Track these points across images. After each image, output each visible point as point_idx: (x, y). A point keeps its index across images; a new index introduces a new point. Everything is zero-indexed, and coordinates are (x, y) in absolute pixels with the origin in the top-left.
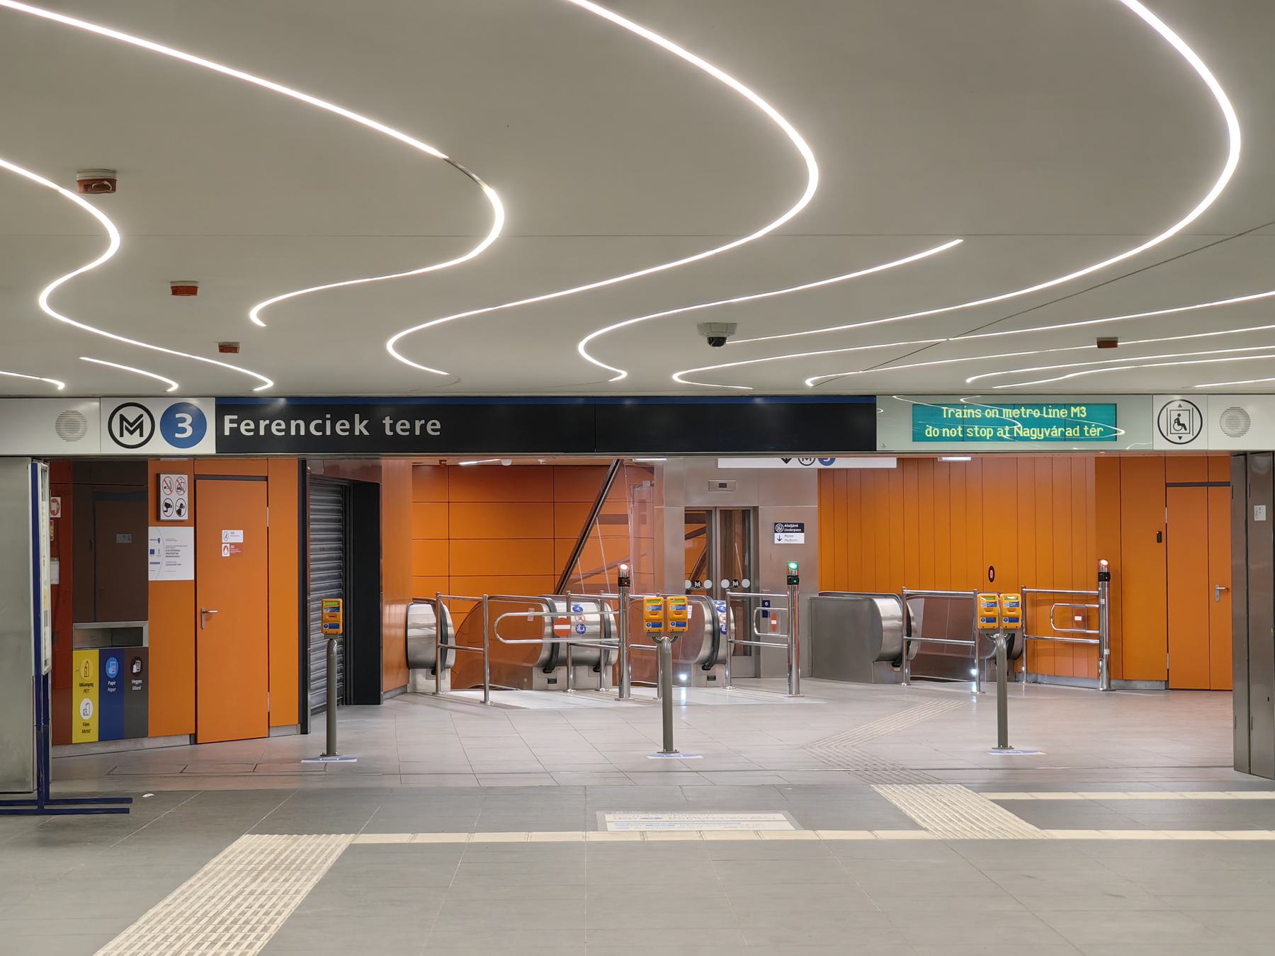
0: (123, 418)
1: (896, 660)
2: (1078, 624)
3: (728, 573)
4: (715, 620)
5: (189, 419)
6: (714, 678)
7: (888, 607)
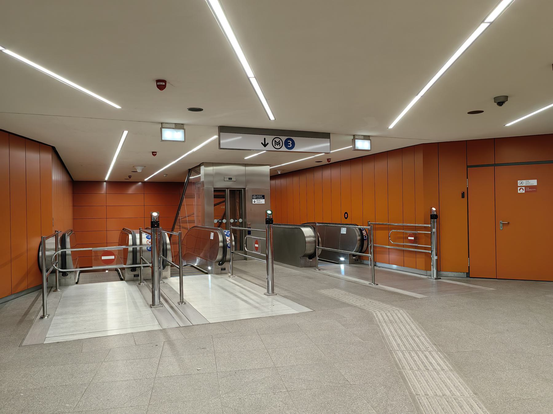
1: (312, 256)
3: (234, 216)
4: (224, 241)
6: (225, 269)
7: (308, 231)
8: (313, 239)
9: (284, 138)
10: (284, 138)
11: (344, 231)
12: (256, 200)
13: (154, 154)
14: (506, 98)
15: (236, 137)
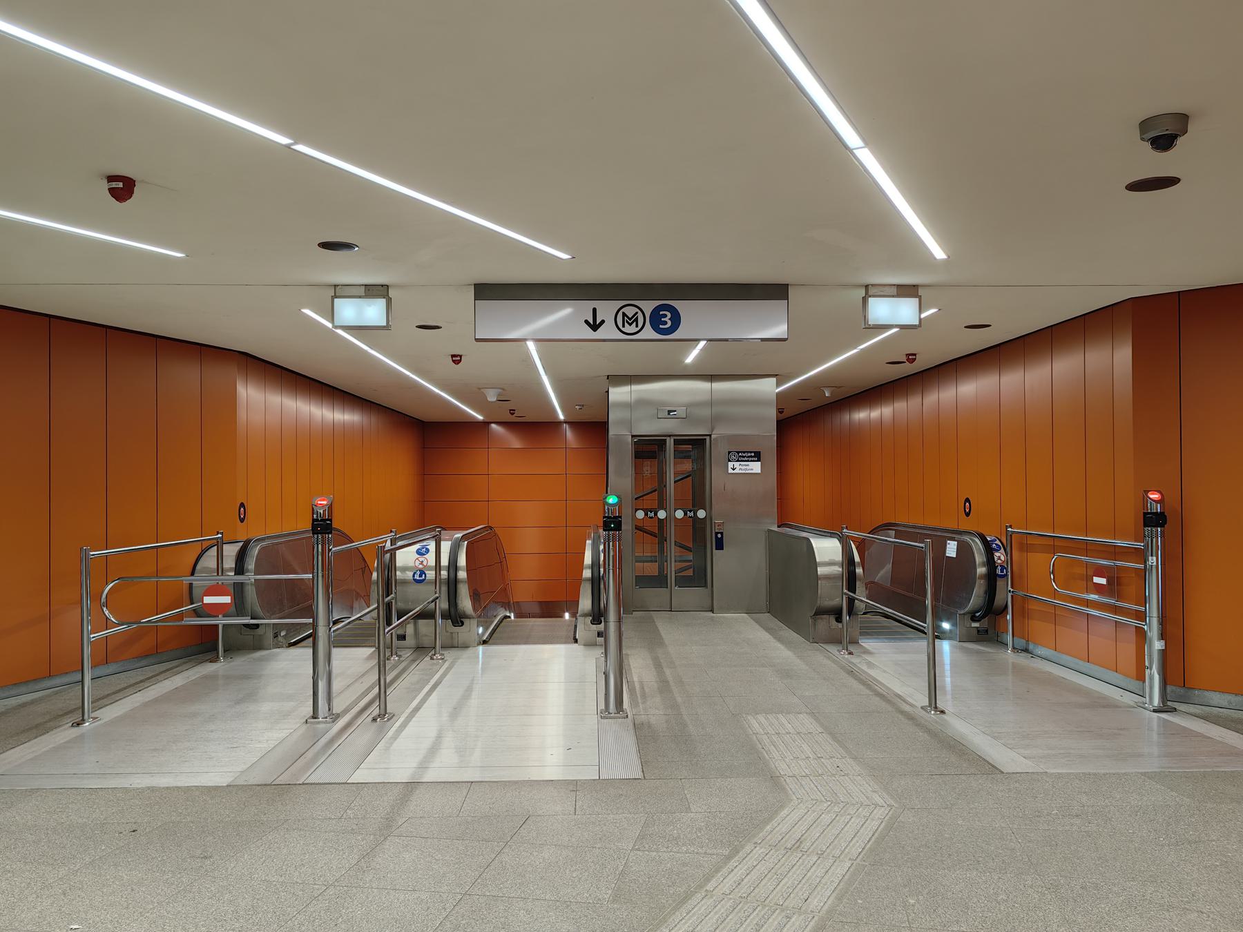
0: (624, 315)
2: (1099, 589)
5: (669, 315)
8: (837, 569)
9: (648, 306)
10: (648, 306)
12: (737, 464)
13: (457, 359)
14: (1182, 120)
15: (564, 308)
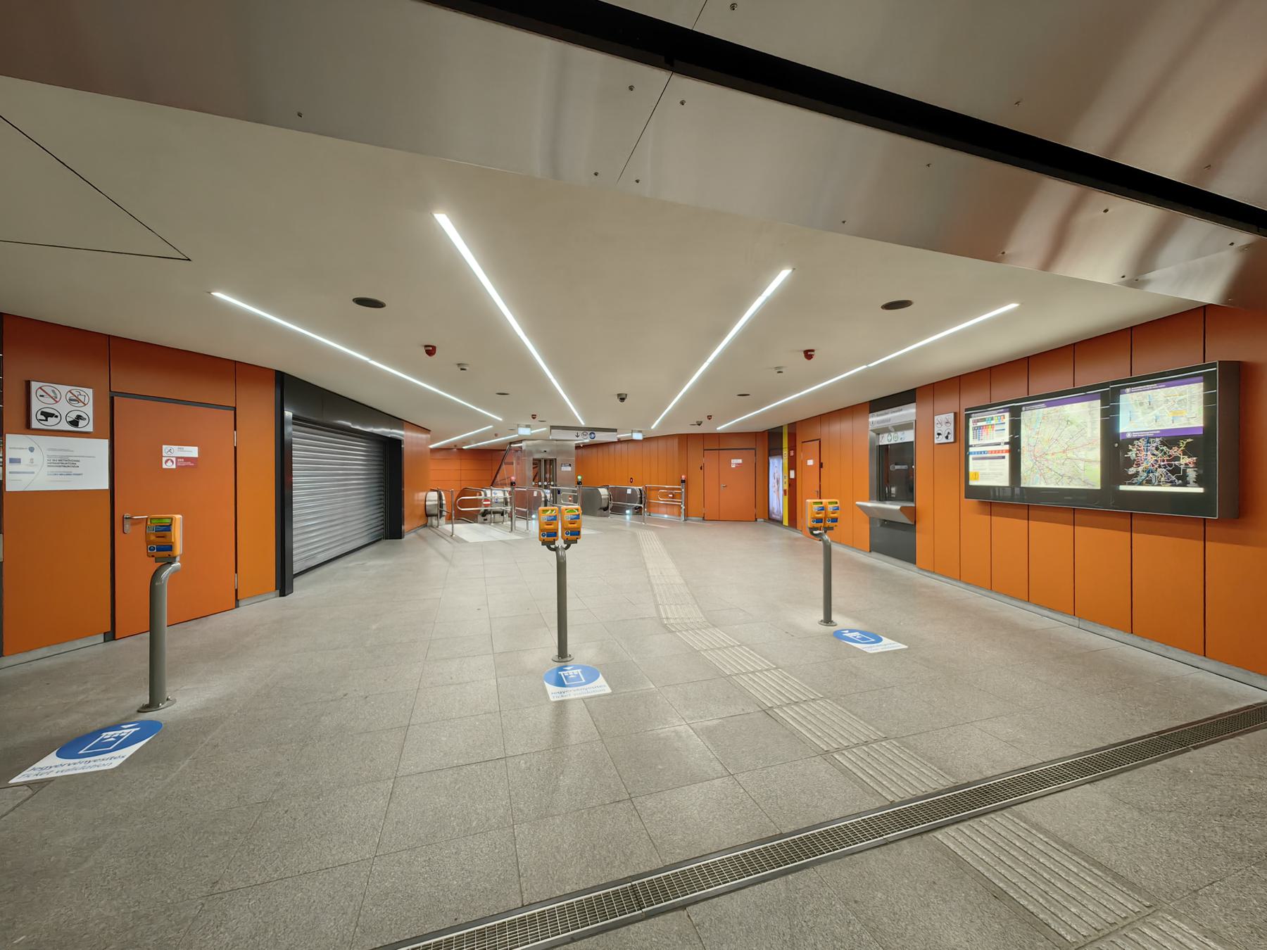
1: (606, 509)
7: (604, 492)
11: (629, 491)
